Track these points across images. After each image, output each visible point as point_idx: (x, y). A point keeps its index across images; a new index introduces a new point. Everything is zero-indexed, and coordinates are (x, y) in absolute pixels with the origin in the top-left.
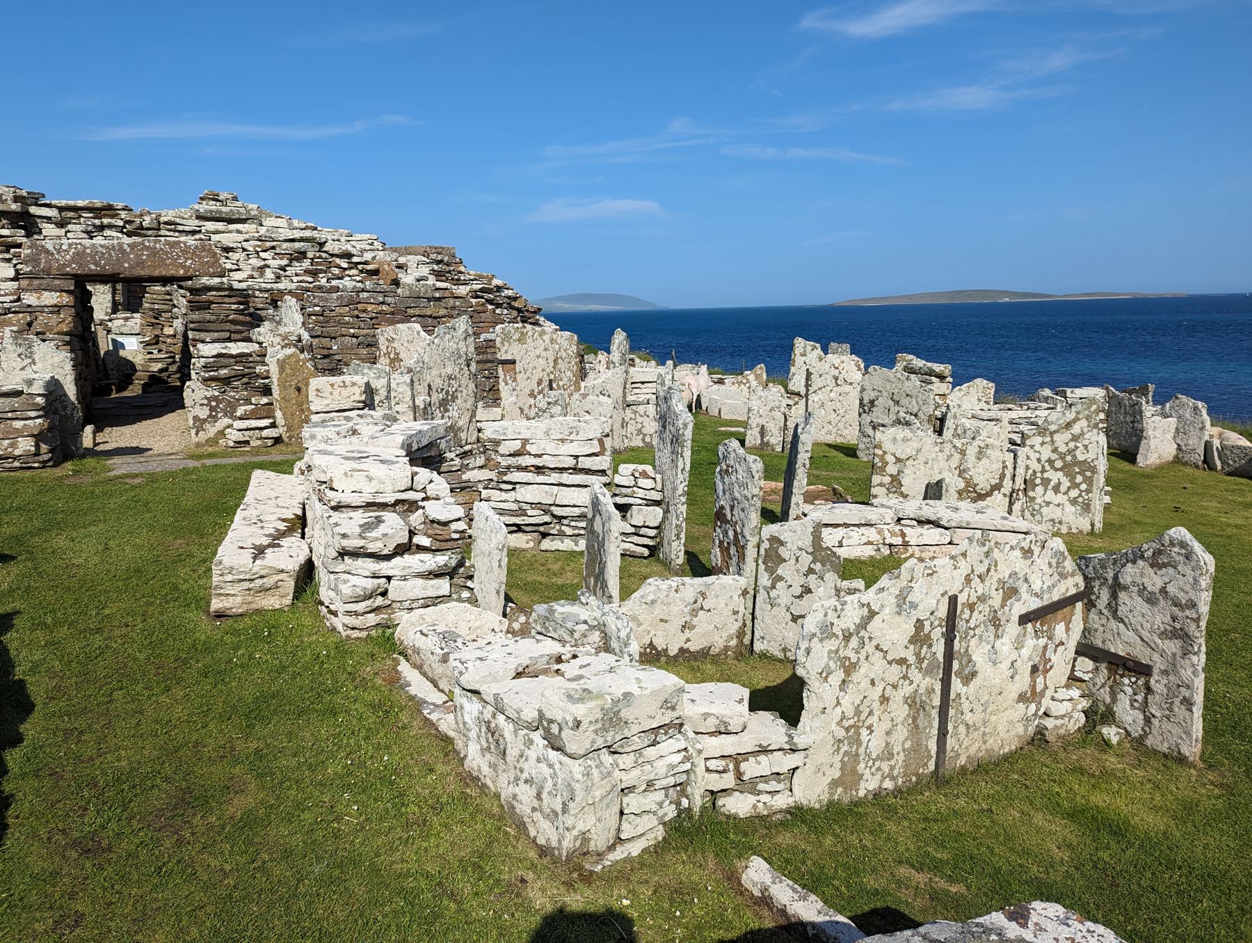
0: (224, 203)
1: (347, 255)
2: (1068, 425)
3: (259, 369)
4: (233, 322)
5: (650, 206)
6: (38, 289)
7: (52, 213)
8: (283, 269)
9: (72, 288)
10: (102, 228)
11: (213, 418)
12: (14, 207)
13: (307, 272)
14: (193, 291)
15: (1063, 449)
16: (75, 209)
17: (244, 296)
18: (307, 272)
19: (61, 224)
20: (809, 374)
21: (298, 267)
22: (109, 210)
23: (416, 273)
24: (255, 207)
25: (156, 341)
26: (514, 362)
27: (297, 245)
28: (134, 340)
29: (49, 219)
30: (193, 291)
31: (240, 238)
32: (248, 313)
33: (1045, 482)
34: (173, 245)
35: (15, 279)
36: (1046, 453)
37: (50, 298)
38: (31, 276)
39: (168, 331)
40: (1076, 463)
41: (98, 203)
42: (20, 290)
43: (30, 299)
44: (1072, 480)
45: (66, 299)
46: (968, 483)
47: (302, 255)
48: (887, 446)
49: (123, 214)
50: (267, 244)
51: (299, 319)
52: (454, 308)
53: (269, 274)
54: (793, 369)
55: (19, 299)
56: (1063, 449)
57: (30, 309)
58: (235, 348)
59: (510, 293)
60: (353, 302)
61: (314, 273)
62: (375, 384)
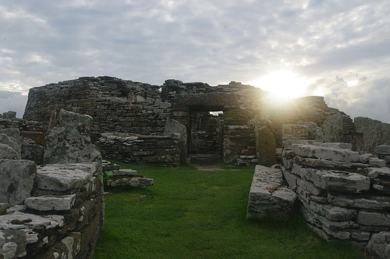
9: (188, 110)
19: (186, 91)
37: (181, 114)
42: (171, 111)
55: (172, 114)
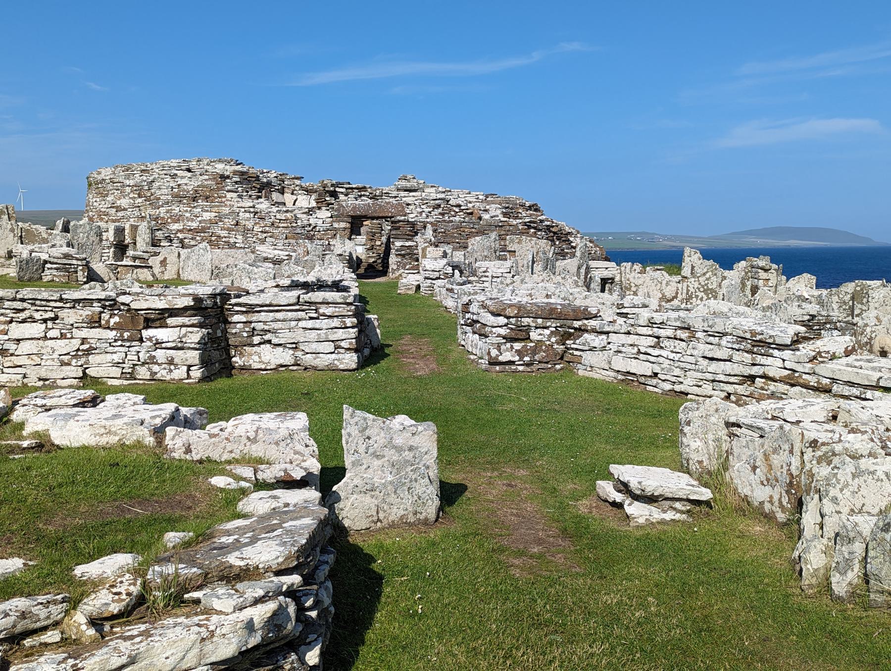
0: (409, 181)
1: (459, 206)
2: (704, 274)
3: (416, 251)
4: (408, 235)
5: (867, 124)
6: (339, 221)
7: (343, 190)
8: (430, 212)
10: (361, 196)
11: (398, 269)
12: (332, 189)
13: (440, 214)
14: (392, 222)
15: (703, 283)
16: (352, 188)
17: (413, 224)
18: (440, 214)
19: (346, 195)
20: (693, 267)
21: (437, 212)
22: (364, 189)
23: (495, 212)
24: (422, 182)
25: (372, 248)
26: (515, 252)
27: (437, 202)
28: (361, 247)
29: (342, 193)
30: (392, 222)
31: (414, 199)
32: (414, 230)
33: (697, 297)
34: (388, 203)
35: (331, 217)
36: (696, 285)
37: (343, 225)
38: (337, 216)
39: (378, 243)
40: (708, 289)
41: (360, 185)
43: (336, 225)
44: (708, 296)
45: (348, 225)
46: (663, 295)
47: (439, 206)
48: (631, 280)
49: (369, 190)
50: (424, 201)
51: (431, 232)
52: (509, 231)
53: (424, 215)
54: (683, 264)
56: (703, 283)
57: (335, 229)
58: (407, 244)
59: (548, 223)
60: (459, 227)
61: (443, 214)
62: (448, 251)
